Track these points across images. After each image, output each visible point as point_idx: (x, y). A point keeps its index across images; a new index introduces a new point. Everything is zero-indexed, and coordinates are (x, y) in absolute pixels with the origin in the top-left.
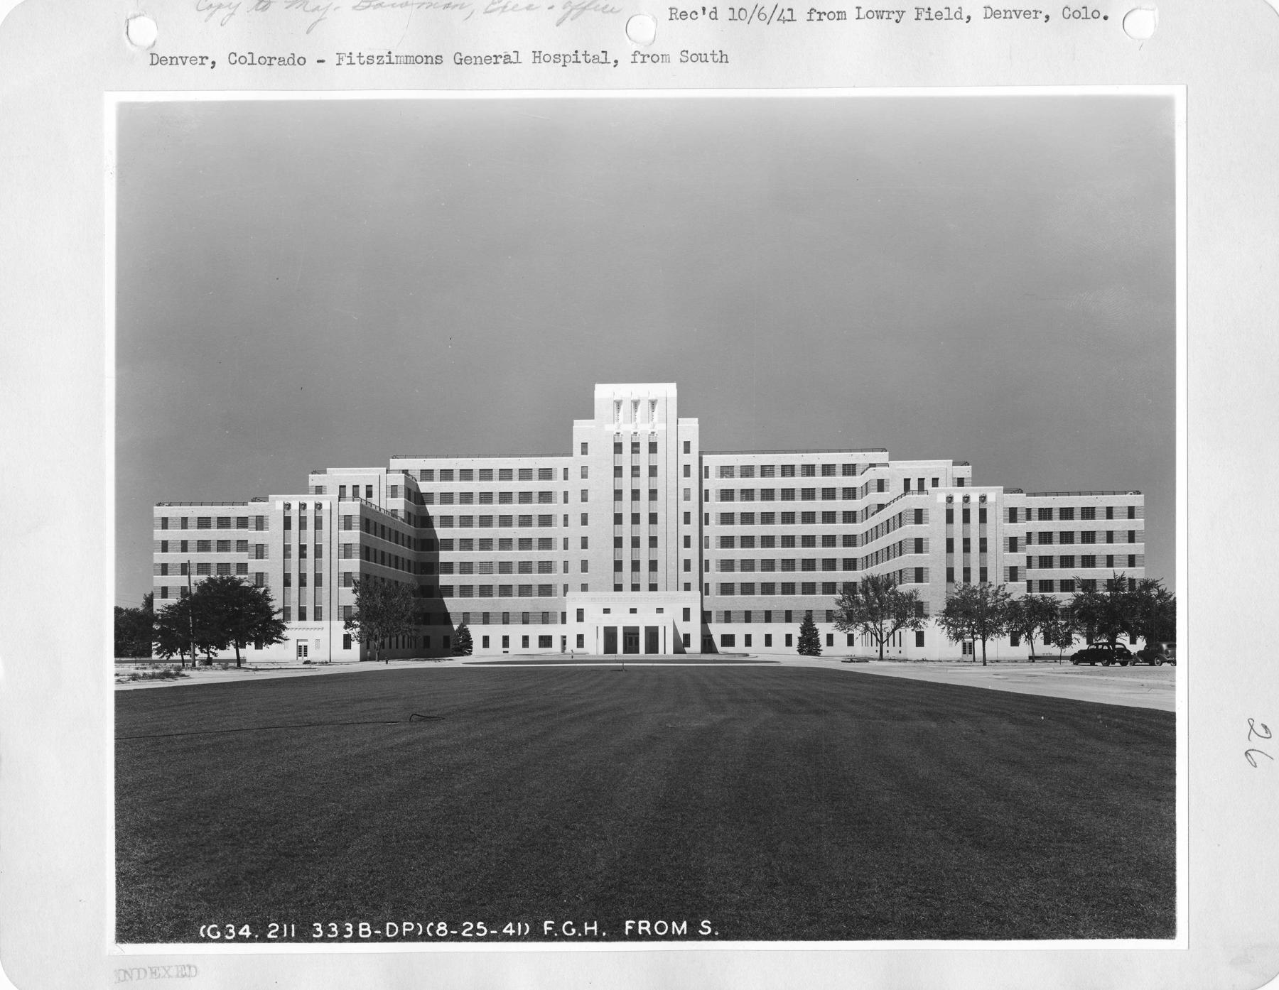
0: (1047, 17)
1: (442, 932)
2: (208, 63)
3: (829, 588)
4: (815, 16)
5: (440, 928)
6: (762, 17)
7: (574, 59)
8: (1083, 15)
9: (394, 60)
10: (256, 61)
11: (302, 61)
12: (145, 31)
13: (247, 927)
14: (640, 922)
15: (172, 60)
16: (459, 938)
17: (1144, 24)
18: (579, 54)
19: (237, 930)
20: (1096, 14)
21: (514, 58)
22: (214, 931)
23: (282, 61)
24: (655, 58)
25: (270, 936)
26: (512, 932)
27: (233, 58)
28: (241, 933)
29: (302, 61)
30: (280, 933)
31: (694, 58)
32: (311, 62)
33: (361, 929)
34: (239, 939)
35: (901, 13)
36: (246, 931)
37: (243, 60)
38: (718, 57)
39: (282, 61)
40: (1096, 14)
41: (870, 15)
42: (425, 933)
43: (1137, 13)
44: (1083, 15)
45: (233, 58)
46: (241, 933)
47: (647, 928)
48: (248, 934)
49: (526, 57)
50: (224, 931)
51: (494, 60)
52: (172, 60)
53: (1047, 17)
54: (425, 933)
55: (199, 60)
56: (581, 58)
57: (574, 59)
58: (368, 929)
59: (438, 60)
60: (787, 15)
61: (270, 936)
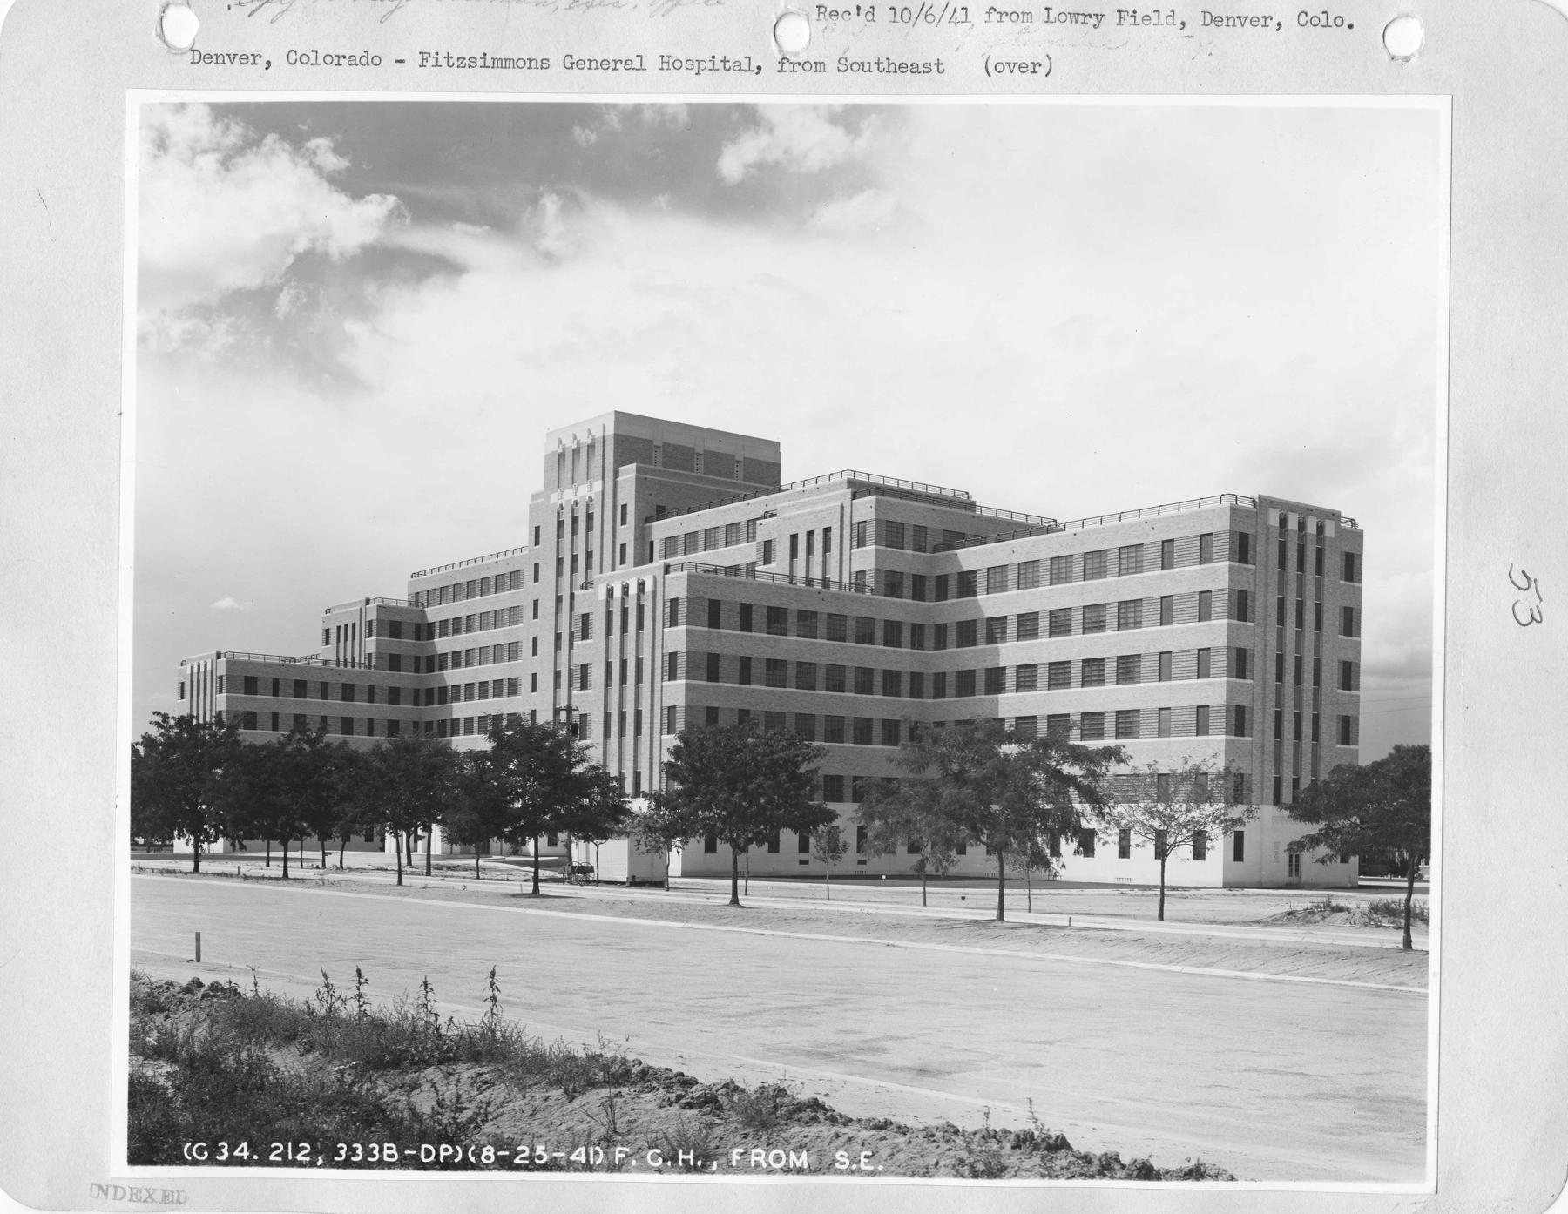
0: (268, 63)
1: (488, 1158)
2: (1272, 24)
3: (891, 732)
4: (995, 16)
5: (485, 1153)
6: (930, 18)
7: (710, 65)
8: (313, 60)
9: (489, 63)
10: (320, 60)
11: (376, 61)
12: (183, 27)
13: (245, 1145)
14: (443, 1146)
15: (218, 59)
16: (264, 1162)
17: (1407, 37)
18: (717, 60)
19: (231, 1151)
20: (1338, 21)
21: (636, 64)
22: (200, 1151)
23: (353, 61)
24: (807, 66)
25: (272, 1158)
26: (246, 1154)
27: (293, 57)
28: (236, 1153)
29: (376, 61)
30: (284, 1155)
31: (855, 67)
32: (388, 61)
33: (386, 1152)
34: (233, 1161)
35: (1099, 17)
36: (243, 1151)
37: (304, 59)
38: (884, 65)
39: (353, 61)
40: (1338, 21)
41: (1063, 17)
42: (465, 1157)
43: (1397, 23)
44: (313, 60)
45: (1303, 19)
46: (236, 1153)
47: (761, 1159)
48: (246, 1154)
49: (652, 62)
50: (214, 1150)
51: (612, 65)
52: (218, 59)
53: (268, 63)
54: (465, 1157)
55: (1262, 21)
56: (719, 65)
57: (710, 65)
58: (394, 1151)
59: (545, 64)
60: (960, 15)
61: (272, 1158)
